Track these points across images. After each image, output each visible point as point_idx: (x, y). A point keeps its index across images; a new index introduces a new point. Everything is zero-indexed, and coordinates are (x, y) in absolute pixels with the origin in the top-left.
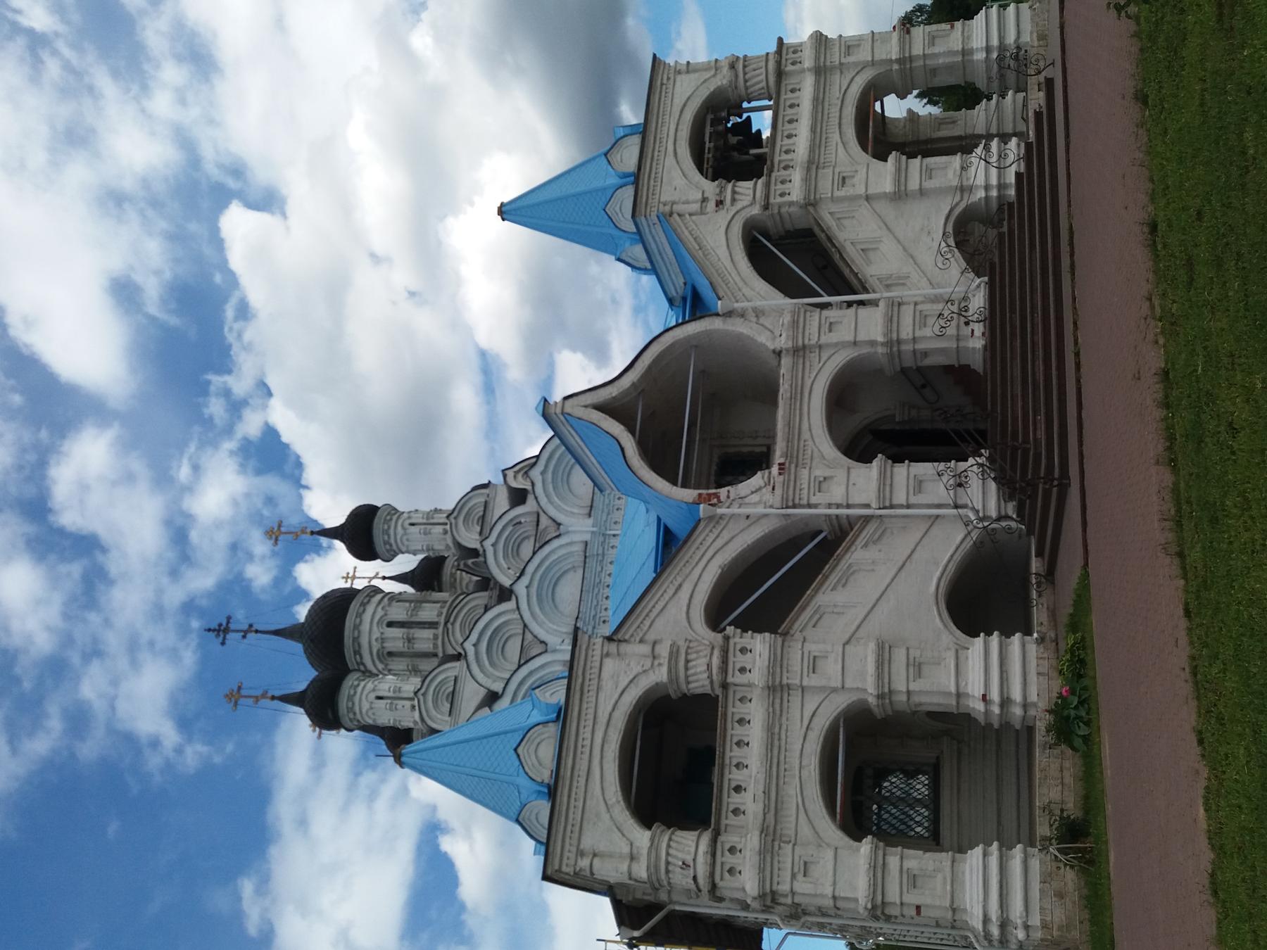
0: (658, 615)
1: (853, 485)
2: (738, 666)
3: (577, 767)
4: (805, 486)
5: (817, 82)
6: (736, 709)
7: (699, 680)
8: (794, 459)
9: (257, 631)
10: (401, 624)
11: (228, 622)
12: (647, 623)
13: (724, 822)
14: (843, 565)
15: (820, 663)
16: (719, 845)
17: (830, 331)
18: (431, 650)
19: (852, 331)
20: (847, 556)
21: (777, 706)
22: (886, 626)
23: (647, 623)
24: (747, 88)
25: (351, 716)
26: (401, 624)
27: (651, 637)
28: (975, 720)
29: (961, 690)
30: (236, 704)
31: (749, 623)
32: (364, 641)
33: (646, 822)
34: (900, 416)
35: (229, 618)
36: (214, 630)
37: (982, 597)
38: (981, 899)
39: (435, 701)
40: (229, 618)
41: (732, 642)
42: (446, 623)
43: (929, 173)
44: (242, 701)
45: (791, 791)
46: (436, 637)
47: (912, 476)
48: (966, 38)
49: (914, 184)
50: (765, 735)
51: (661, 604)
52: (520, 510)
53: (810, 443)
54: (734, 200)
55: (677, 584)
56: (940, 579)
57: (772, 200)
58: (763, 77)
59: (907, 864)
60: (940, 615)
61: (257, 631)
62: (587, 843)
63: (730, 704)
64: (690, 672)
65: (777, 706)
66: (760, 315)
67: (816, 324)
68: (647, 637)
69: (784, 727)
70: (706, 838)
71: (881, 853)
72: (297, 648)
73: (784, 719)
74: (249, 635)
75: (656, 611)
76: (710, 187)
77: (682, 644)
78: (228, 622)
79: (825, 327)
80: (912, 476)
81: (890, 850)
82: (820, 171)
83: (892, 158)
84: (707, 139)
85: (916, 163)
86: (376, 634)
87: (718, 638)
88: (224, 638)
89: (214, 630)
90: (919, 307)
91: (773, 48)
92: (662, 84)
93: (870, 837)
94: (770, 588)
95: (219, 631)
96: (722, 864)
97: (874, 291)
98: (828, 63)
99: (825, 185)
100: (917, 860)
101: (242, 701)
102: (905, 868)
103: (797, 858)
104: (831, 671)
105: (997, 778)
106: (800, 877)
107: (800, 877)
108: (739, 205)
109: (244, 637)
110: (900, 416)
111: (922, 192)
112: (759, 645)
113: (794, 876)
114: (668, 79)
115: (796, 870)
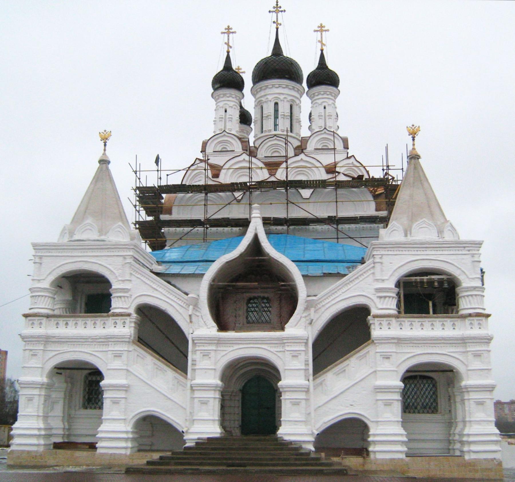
0: (142, 280)
1: (208, 367)
2: (117, 321)
3: (75, 251)
4: (206, 348)
5: (457, 339)
6: (448, 322)
7: (117, 305)
8: (219, 342)
9: (277, 29)
10: (276, 111)
11: (282, 11)
12: (139, 276)
13: (53, 319)
14: (166, 368)
15: (206, 357)
16: (42, 318)
17: (293, 356)
18: (264, 129)
19: (293, 369)
20: (170, 369)
21: (100, 340)
22: (139, 388)
23: (139, 276)
24: (464, 297)
25: (316, 94)
26: (276, 111)
27: (133, 278)
28: (100, 426)
29: (49, 418)
30: (224, 33)
31: (140, 326)
32: (268, 91)
33: (398, 285)
34: (253, 393)
35: (328, 30)
36: (277, 5)
37: (152, 427)
38: (22, 427)
39: (220, 142)
40: (328, 30)
41: (128, 318)
42: (275, 135)
43: (388, 404)
44: (226, 35)
45: (65, 348)
46: (270, 131)
47: (209, 399)
48: (479, 422)
49: (197, 394)
50: (27, 335)
51: (148, 282)
52: (323, 171)
53: (231, 349)
54: (381, 297)
55: (158, 288)
56: (157, 412)
57: (376, 319)
58: (466, 307)
59: (36, 398)
60: (350, 413)
61: (277, 29)
62: (45, 260)
63: (440, 319)
64: (466, 297)
65: (100, 340)
66: (303, 327)
67: (297, 348)
68: (133, 276)
69: (92, 344)
70: (395, 312)
71: (398, 390)
72: (221, 68)
73: (95, 343)
74: (275, 25)
75: (144, 279)
76: (391, 284)
77: (130, 293)
78: (282, 11)
79: (295, 354)
80: (484, 400)
81: (399, 394)
82: (394, 345)
83: (402, 385)
84: (429, 277)
85: (398, 397)
86: (270, 97)
87: (132, 311)
88: (272, 12)
89: (277, 5)
90: (303, 402)
91: (486, 312)
92: (464, 247)
93: (403, 385)
94: (160, 336)
95: (277, 8)
96: (404, 321)
97: (314, 379)
98: (468, 344)
99: (381, 349)
100: (397, 407)
101: (226, 35)
102: (35, 396)
103: (37, 351)
104: (117, 364)
105: (434, 440)
106: (31, 353)
107: (31, 353)
108: (377, 300)
109: (274, 22)
110: (253, 393)
111: (193, 398)
112: (127, 329)
113: (31, 350)
114: (469, 250)
115: (34, 351)
